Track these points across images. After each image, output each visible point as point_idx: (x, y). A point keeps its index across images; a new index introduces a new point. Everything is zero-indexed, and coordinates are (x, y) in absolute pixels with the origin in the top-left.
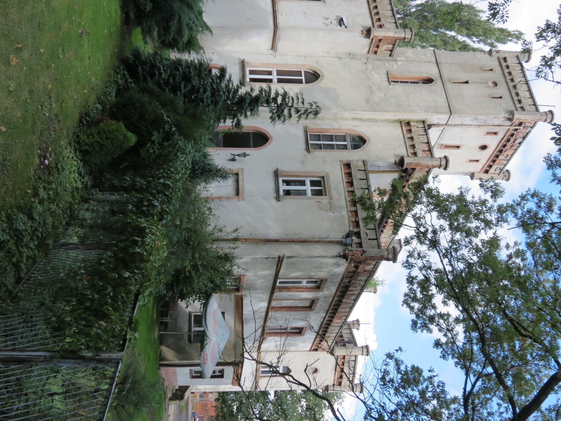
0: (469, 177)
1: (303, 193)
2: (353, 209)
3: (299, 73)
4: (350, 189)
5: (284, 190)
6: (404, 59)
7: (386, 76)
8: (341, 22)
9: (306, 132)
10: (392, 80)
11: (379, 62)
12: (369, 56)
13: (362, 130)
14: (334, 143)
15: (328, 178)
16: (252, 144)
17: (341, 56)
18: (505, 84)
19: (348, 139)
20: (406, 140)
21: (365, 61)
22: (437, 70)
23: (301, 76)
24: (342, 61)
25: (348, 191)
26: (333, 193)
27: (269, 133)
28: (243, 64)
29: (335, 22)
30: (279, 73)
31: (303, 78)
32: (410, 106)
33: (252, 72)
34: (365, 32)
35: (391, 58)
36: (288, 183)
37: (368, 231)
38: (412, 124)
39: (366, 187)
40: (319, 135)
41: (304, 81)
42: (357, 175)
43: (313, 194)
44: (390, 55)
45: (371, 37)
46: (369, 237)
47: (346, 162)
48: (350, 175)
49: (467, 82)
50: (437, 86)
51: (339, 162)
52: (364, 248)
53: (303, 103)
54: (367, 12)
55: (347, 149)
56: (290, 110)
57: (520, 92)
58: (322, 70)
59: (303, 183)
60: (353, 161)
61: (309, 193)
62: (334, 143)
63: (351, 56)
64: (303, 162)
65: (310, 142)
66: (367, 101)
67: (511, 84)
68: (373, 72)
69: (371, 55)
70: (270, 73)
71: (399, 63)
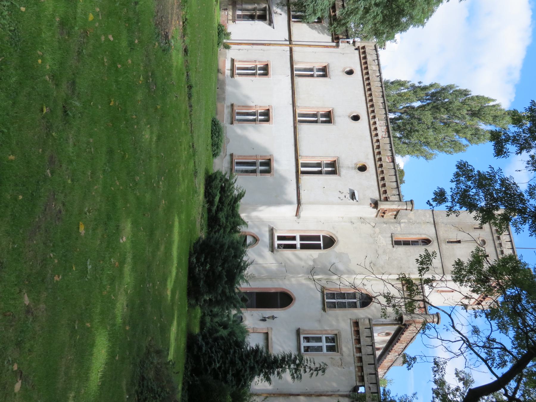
2: (359, 364)
3: (317, 238)
4: (358, 346)
5: (304, 347)
6: (406, 221)
7: (391, 239)
8: (353, 196)
9: (323, 292)
11: (385, 225)
12: (377, 219)
14: (346, 301)
15: (340, 336)
16: (279, 305)
17: (353, 221)
18: (492, 242)
21: (374, 225)
22: (434, 231)
23: (320, 241)
24: (354, 225)
25: (356, 348)
27: (293, 294)
28: (272, 231)
29: (348, 196)
30: (302, 238)
31: (321, 242)
32: (409, 268)
33: (280, 238)
34: (373, 205)
35: (395, 220)
36: (308, 339)
37: (371, 386)
39: (370, 344)
40: (334, 293)
41: (322, 245)
42: (364, 334)
43: (327, 350)
44: (395, 218)
45: (378, 209)
46: (372, 391)
47: (355, 320)
48: (357, 332)
49: (459, 242)
51: (349, 321)
53: (314, 364)
54: (376, 184)
55: (356, 307)
56: (305, 367)
57: (504, 250)
58: (337, 235)
59: (319, 339)
60: (361, 319)
61: (324, 339)
62: (346, 301)
63: (362, 220)
67: (497, 242)
68: (380, 236)
69: (379, 219)
70: (294, 238)
71: (402, 225)
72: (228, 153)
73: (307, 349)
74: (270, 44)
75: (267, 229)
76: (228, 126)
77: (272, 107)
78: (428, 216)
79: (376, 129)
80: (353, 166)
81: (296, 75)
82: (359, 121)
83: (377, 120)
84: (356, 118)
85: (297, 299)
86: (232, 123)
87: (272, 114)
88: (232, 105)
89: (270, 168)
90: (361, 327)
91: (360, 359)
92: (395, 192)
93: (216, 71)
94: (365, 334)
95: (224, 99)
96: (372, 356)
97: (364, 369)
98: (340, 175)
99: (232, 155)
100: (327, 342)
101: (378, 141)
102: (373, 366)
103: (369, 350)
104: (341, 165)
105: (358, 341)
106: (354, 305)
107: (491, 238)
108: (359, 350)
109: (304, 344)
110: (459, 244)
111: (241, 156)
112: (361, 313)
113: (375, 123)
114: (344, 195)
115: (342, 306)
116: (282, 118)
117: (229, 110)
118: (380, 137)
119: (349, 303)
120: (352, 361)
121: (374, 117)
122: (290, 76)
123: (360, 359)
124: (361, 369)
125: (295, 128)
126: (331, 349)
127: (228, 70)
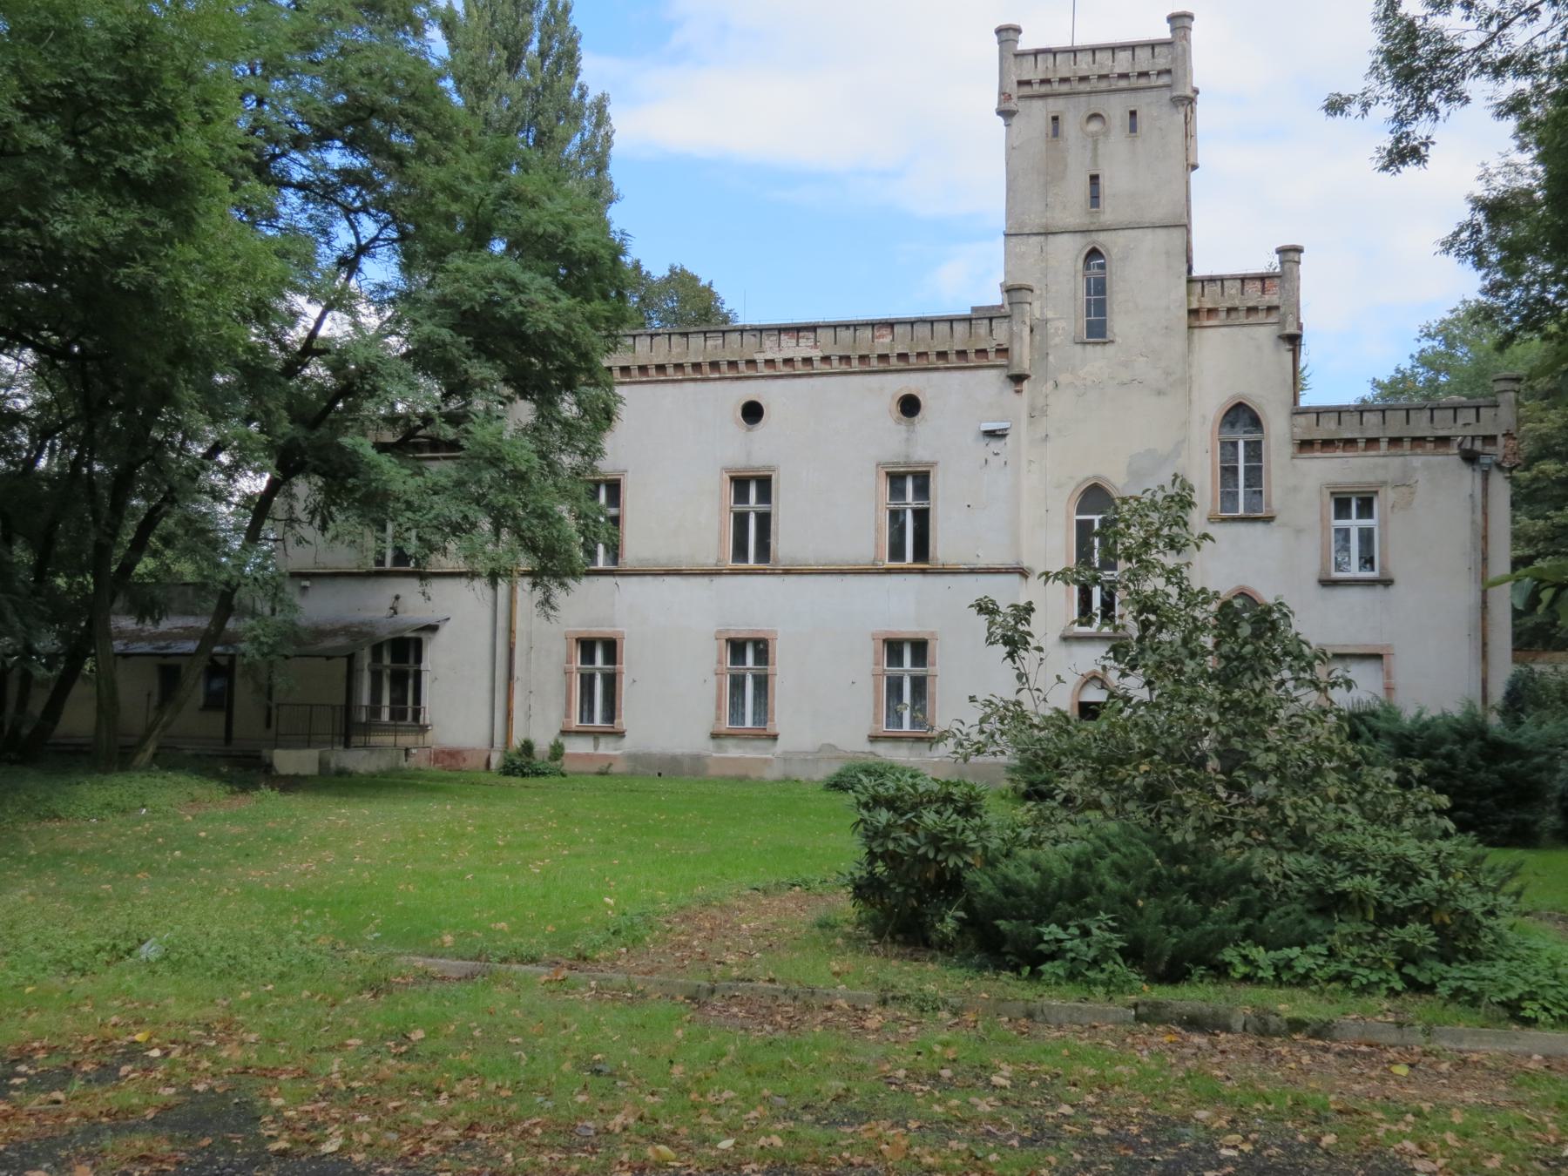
0: (1194, 174)
1: (1366, 537)
2: (1407, 445)
3: (1084, 529)
10: (1097, 331)
11: (1051, 358)
13: (1212, 404)
15: (1335, 485)
18: (1093, 98)
19: (1230, 436)
20: (1229, 322)
22: (1066, 237)
23: (1092, 522)
25: (1366, 449)
26: (1370, 478)
29: (995, 445)
32: (1168, 308)
37: (1460, 422)
38: (1195, 306)
39: (1357, 416)
43: (1370, 516)
47: (1295, 449)
48: (1328, 444)
49: (1094, 179)
50: (1112, 243)
52: (1499, 433)
57: (1118, 70)
59: (1344, 534)
61: (1366, 523)
64: (1299, 531)
65: (1241, 512)
66: (1160, 393)
68: (1081, 373)
71: (1050, 315)
72: (868, 747)
73: (1367, 561)
74: (511, 631)
75: (1063, 651)
76: (781, 746)
77: (719, 632)
78: (1023, 248)
79: (788, 361)
80: (903, 428)
81: (615, 562)
82: (763, 403)
83: (760, 357)
84: (752, 412)
85: (1242, 583)
86: (620, 735)
87: (742, 630)
88: (715, 736)
89: (907, 640)
90: (1319, 434)
91: (1395, 441)
92: (942, 328)
93: (606, 779)
94: (1333, 425)
95: (697, 759)
96: (1388, 413)
97: (1419, 434)
98: (934, 464)
99: (874, 739)
100: (1349, 517)
101: (826, 359)
102: (1412, 413)
103: (1372, 419)
104: (902, 460)
105: (1350, 443)
106: (1254, 450)
107: (1083, 99)
108: (1372, 442)
109: (1354, 571)
110: (1101, 180)
111: (875, 715)
112: (1278, 431)
113: (770, 363)
114: (991, 458)
115: (1255, 475)
116: (753, 603)
117: (729, 743)
118: (816, 354)
119: (1247, 459)
120: (1397, 461)
121: (751, 363)
122: (619, 580)
123: (1395, 441)
124: (1418, 441)
125: (787, 572)
126: (1366, 508)
127: (596, 747)
